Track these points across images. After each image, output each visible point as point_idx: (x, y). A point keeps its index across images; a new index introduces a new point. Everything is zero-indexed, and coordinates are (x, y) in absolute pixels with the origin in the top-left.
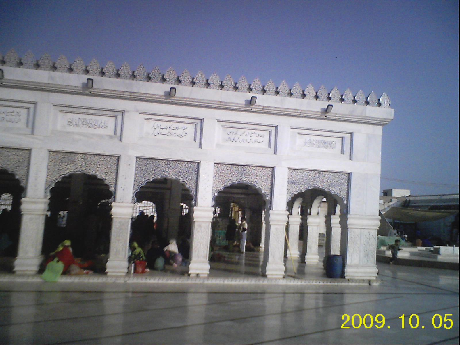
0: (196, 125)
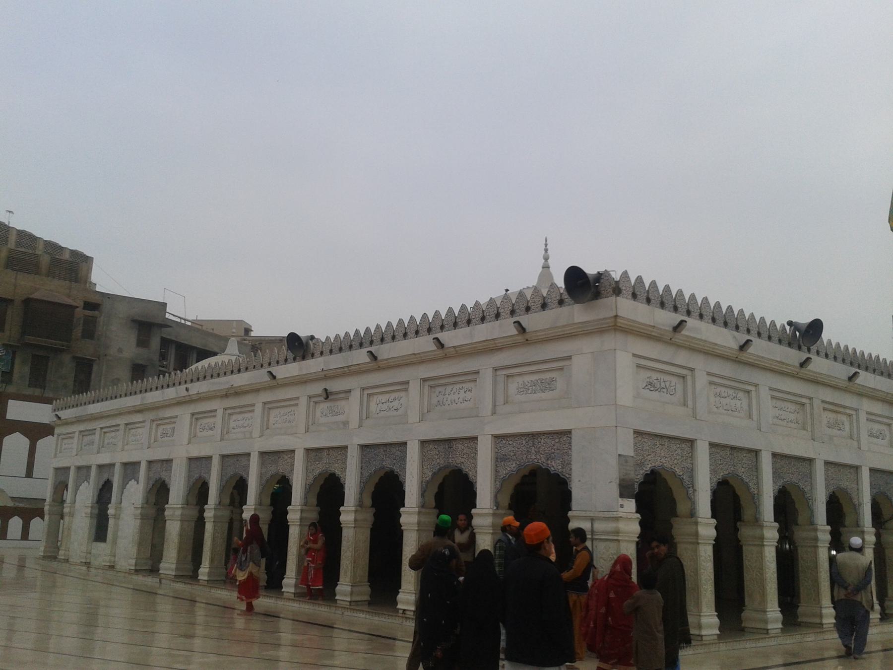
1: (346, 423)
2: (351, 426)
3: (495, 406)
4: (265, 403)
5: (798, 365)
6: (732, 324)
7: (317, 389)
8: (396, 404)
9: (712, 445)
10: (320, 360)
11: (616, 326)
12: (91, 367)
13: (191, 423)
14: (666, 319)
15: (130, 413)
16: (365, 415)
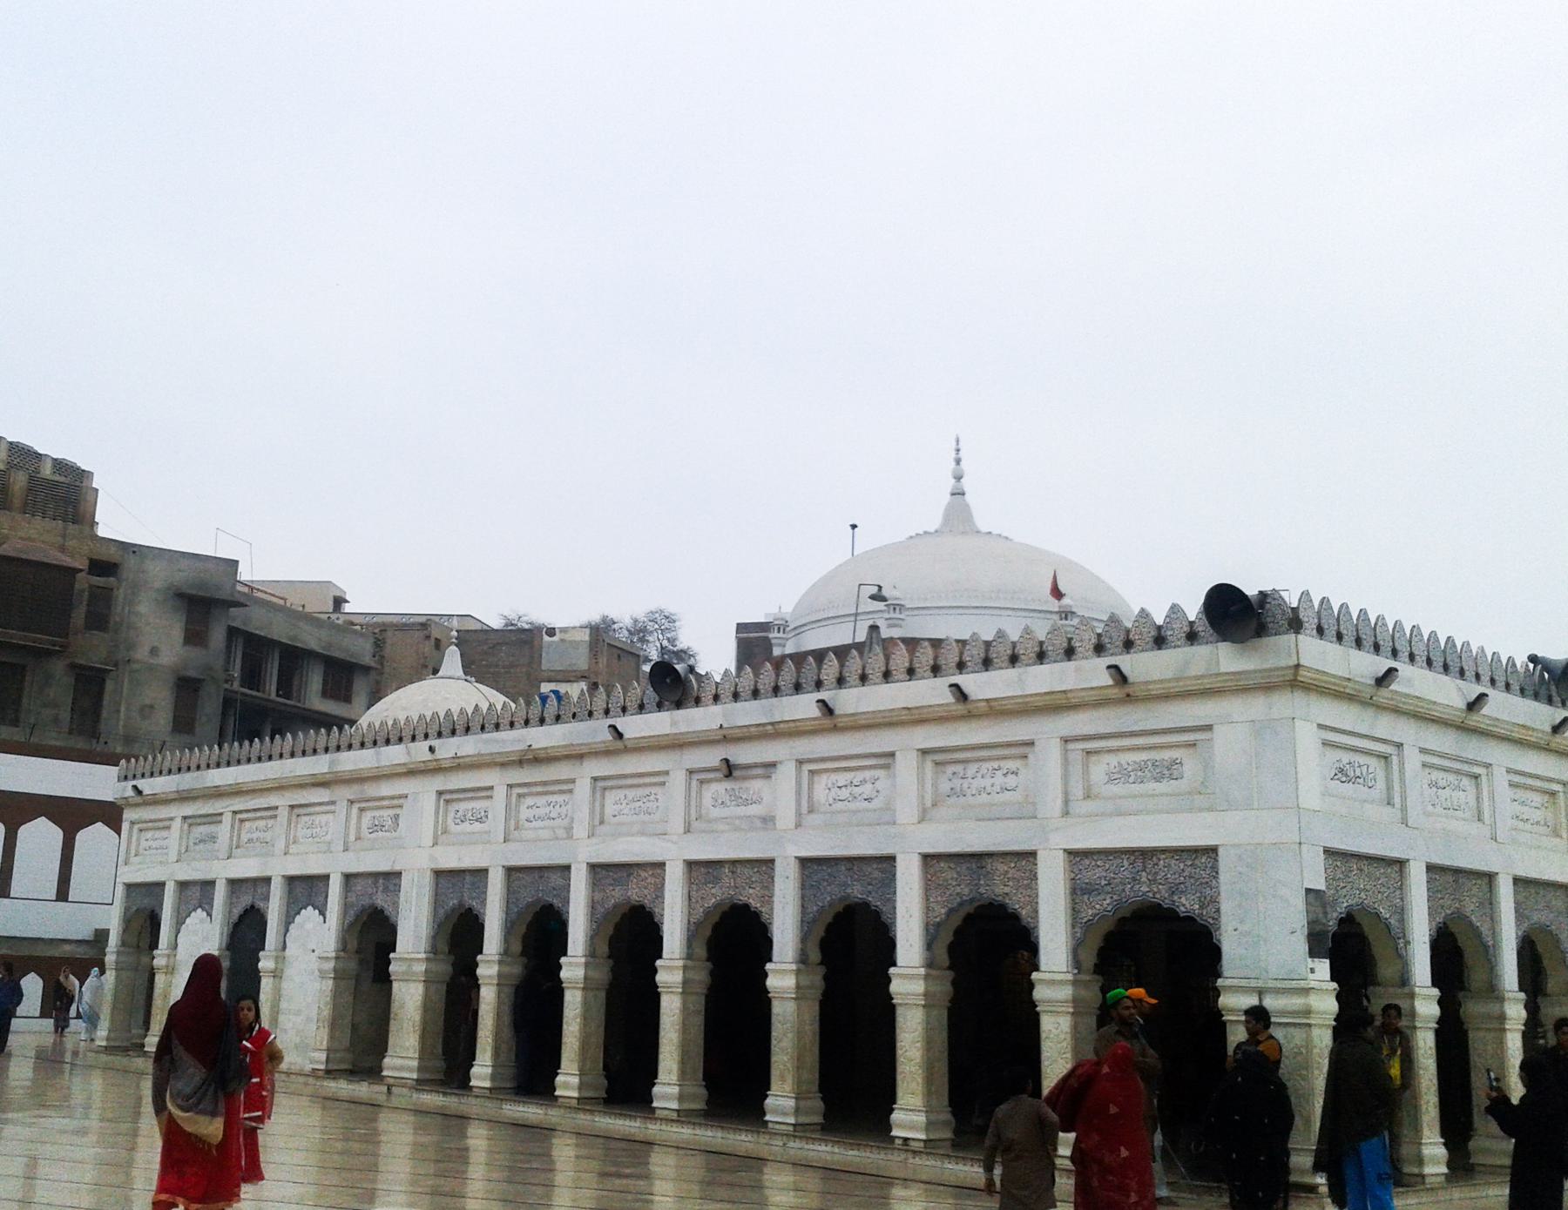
0: (242, 821)
1: (768, 821)
2: (780, 824)
3: (1066, 802)
4: (595, 779)
5: (1548, 729)
6: (1438, 661)
7: (711, 757)
8: (867, 789)
9: (1431, 868)
10: (716, 709)
11: (1295, 680)
12: (102, 684)
13: (438, 808)
14: (1365, 665)
15: (302, 786)
16: (807, 809)
